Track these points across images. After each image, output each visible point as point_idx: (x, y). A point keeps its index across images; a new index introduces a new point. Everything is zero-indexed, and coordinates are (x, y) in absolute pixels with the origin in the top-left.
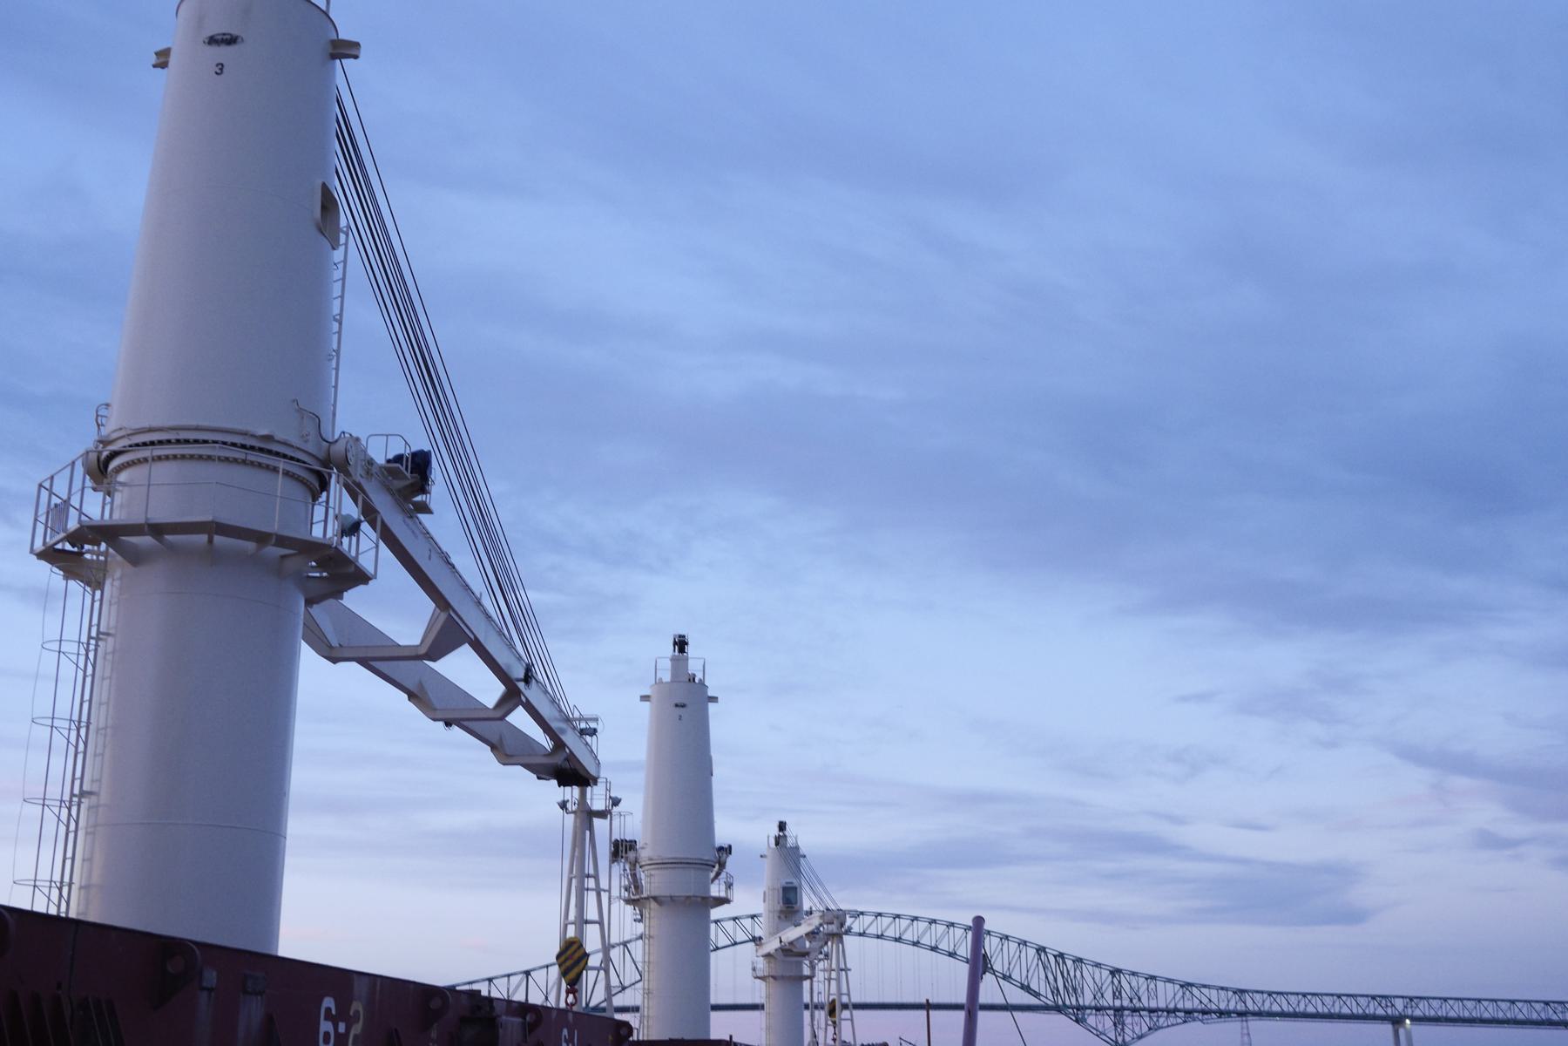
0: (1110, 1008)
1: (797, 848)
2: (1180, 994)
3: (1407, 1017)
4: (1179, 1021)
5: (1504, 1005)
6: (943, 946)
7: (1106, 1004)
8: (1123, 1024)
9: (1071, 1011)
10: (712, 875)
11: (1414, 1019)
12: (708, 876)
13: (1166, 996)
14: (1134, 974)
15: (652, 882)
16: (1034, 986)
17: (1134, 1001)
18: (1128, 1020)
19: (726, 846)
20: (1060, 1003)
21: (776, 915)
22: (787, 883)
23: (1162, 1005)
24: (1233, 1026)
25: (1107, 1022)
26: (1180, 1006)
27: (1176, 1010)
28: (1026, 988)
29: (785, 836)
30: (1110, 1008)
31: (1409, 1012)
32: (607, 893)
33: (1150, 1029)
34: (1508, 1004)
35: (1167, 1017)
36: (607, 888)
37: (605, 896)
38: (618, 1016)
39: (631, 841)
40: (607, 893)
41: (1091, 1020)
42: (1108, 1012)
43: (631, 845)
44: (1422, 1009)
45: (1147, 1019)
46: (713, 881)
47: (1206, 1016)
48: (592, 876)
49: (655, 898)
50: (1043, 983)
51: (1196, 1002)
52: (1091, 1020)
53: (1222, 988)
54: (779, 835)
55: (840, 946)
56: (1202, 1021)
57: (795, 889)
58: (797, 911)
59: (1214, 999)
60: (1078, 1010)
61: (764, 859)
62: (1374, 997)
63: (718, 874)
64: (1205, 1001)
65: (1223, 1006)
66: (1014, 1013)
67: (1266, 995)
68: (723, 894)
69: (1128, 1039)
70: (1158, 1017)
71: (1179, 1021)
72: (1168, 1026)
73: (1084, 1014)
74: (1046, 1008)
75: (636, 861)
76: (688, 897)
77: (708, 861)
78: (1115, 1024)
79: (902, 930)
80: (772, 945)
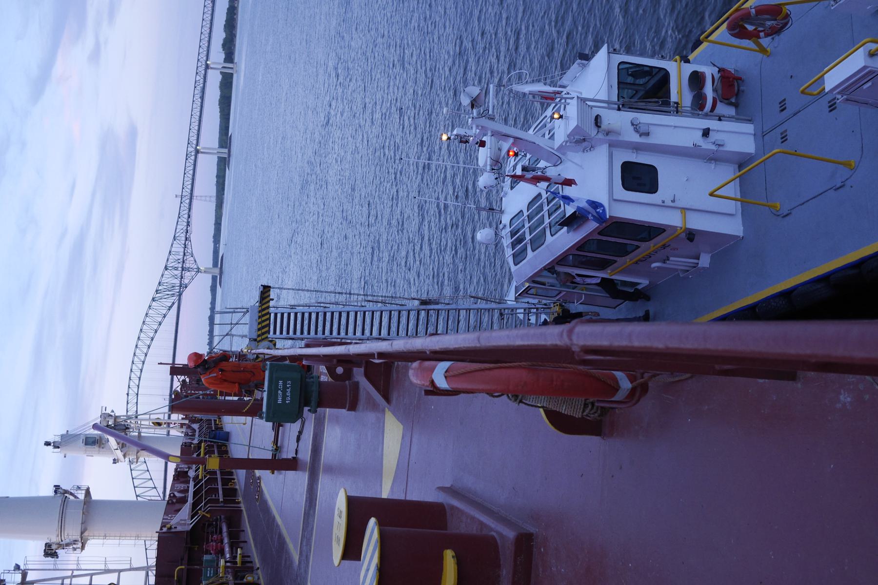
0: (182, 273)
1: (62, 436)
2: (178, 241)
3: (196, 148)
4: (190, 243)
5: (203, 37)
6: (148, 343)
7: (180, 274)
8: (189, 268)
9: (181, 289)
10: (72, 498)
11: (207, 60)
12: (72, 501)
13: (178, 248)
14: (168, 260)
15: (72, 532)
16: (170, 304)
17: (180, 261)
18: (188, 265)
19: (54, 489)
20: (178, 294)
21: (101, 449)
22: (83, 443)
23: (182, 250)
24: (194, 202)
25: (187, 274)
26: (183, 242)
27: (185, 244)
28: (170, 307)
29: (54, 442)
30: (182, 273)
31: (194, 146)
32: (74, 571)
33: (192, 256)
34: (201, 48)
35: (188, 248)
36: (71, 572)
37: (76, 573)
38: (167, 498)
39: (45, 547)
40: (74, 571)
41: (186, 281)
42: (183, 273)
43: (48, 546)
44: (193, 140)
45: (188, 257)
46: (76, 497)
47: (189, 232)
48: (63, 581)
49: (82, 533)
50: (168, 300)
51: (182, 235)
52: (186, 281)
53: (177, 223)
54: (53, 446)
55: (122, 417)
56: (190, 234)
57: (87, 438)
58: (100, 437)
59: (182, 227)
60: (181, 286)
61: (67, 456)
62: (187, 159)
63: (72, 494)
64: (182, 231)
65: (185, 224)
66: (168, 407)
67: (180, 220)
68: (84, 492)
69: (196, 267)
70: (187, 252)
71: (190, 243)
72: (192, 248)
73: (183, 284)
74: (179, 300)
75: (59, 544)
76: (83, 513)
77: (62, 501)
78: (189, 271)
79: (715, 193)
80: (119, 454)
